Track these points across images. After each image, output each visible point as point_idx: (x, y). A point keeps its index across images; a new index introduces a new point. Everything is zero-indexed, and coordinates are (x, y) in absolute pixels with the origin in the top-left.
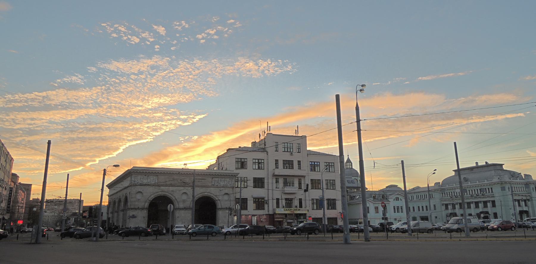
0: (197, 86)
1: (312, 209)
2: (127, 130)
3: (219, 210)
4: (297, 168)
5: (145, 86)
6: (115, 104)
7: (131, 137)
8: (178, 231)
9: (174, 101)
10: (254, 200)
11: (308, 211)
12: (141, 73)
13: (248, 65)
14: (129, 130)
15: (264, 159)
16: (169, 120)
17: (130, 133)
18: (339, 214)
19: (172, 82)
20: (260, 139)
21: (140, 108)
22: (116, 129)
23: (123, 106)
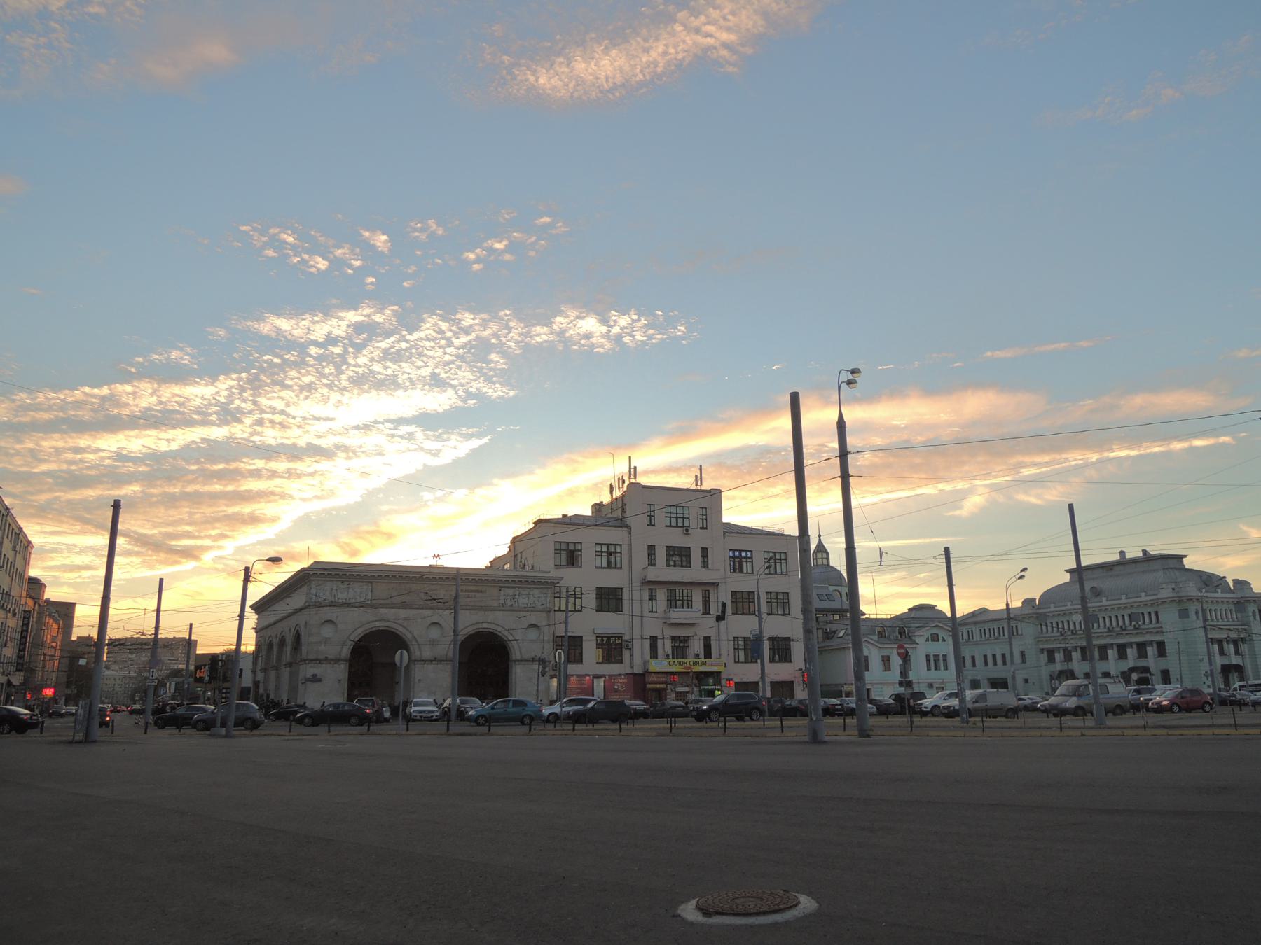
1: (735, 662)
8: (420, 712)
10: (597, 640)
12: (331, 340)
18: (799, 674)
20: (612, 496)
21: (329, 424)
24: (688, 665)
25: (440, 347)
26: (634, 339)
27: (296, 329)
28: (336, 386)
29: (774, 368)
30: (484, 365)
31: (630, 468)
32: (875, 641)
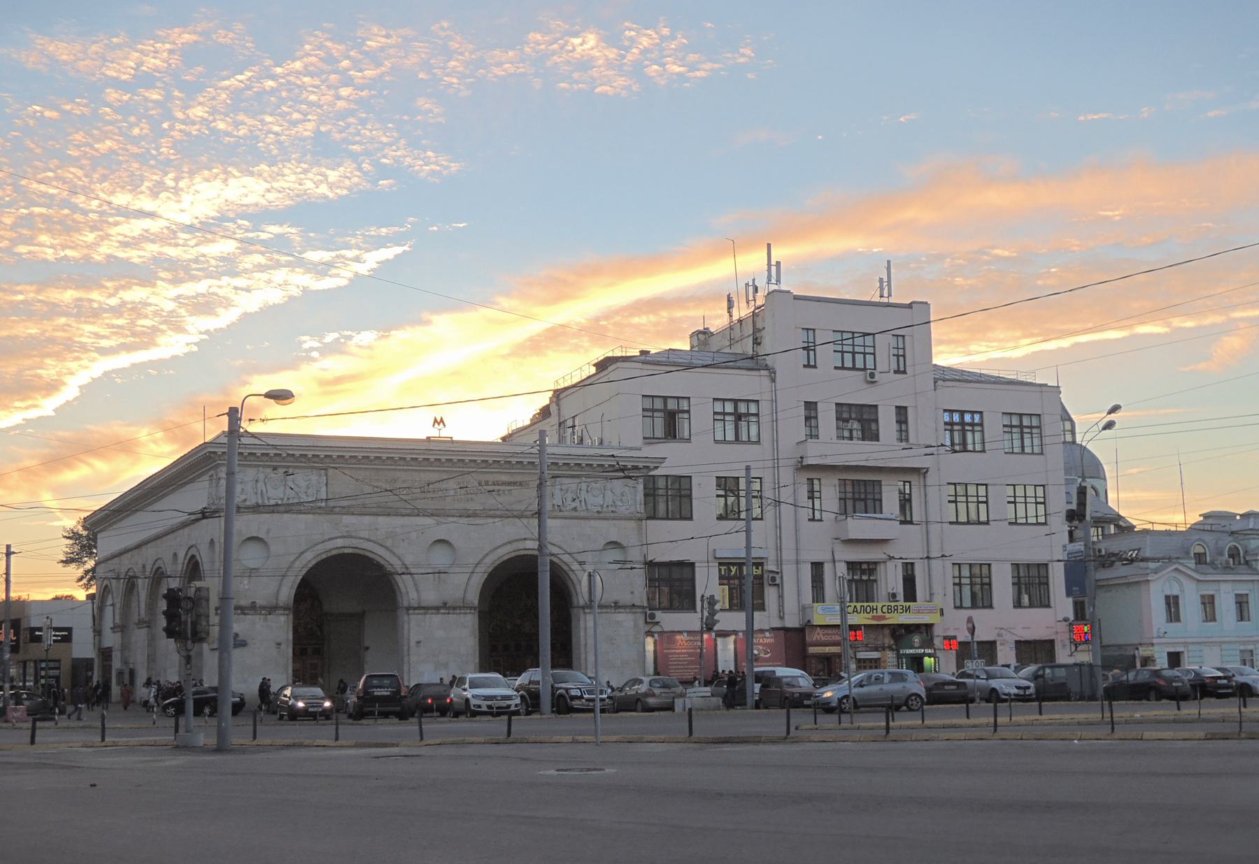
0: (371, 131)
1: (956, 607)
2: (94, 314)
3: (585, 613)
4: (895, 435)
5: (164, 134)
6: (49, 207)
7: (114, 338)
8: (487, 698)
9: (280, 195)
10: (720, 570)
11: (942, 613)
12: (144, 80)
13: (577, 41)
14: (106, 311)
15: (757, 401)
16: (261, 268)
17: (107, 321)
18: (1063, 627)
19: (271, 115)
20: (731, 316)
21: (146, 223)
22: (54, 309)
23: (78, 217)
24: (880, 613)
25: (329, 87)
26: (665, 70)
27: (84, 60)
28: (154, 157)
29: (902, 119)
30: (406, 118)
31: (769, 264)
32: (1192, 570)
